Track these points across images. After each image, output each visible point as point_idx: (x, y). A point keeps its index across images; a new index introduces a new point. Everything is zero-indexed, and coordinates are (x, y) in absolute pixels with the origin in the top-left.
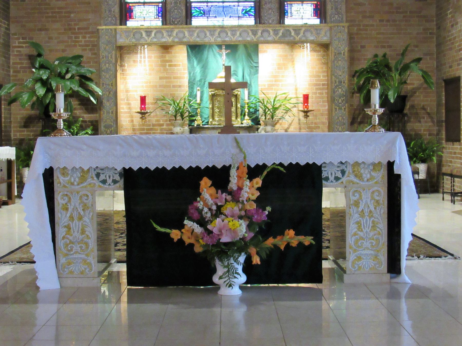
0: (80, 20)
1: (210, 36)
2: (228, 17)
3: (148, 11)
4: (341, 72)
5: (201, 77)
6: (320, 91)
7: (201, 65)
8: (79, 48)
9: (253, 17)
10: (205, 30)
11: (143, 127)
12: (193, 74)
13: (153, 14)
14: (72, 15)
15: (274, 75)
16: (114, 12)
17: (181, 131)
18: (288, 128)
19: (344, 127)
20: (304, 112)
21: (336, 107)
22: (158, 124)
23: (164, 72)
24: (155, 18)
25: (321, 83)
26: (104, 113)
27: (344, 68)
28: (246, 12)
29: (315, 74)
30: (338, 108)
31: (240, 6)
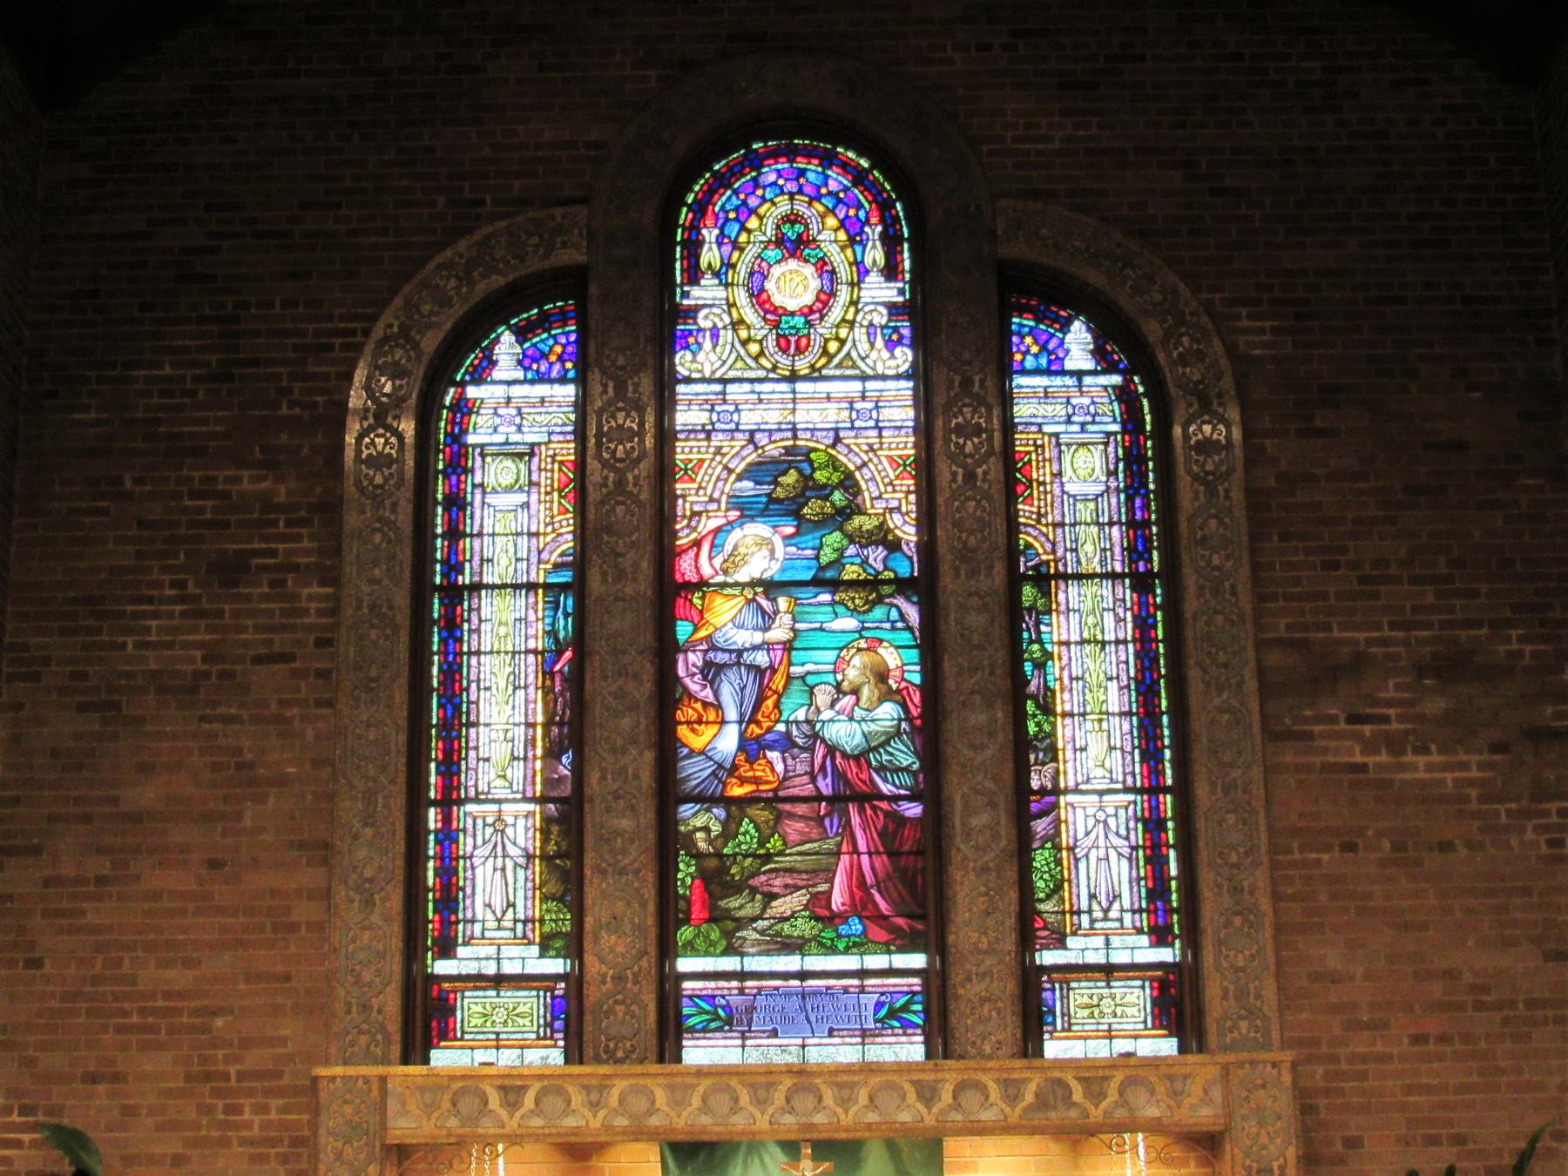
0: (246, 1044)
1: (751, 1108)
3: (511, 1007)
8: (240, 1149)
9: (919, 1031)
10: (734, 1082)
13: (532, 1021)
14: (219, 1022)
16: (379, 1011)
24: (538, 1038)
28: (892, 1014)
31: (867, 989)
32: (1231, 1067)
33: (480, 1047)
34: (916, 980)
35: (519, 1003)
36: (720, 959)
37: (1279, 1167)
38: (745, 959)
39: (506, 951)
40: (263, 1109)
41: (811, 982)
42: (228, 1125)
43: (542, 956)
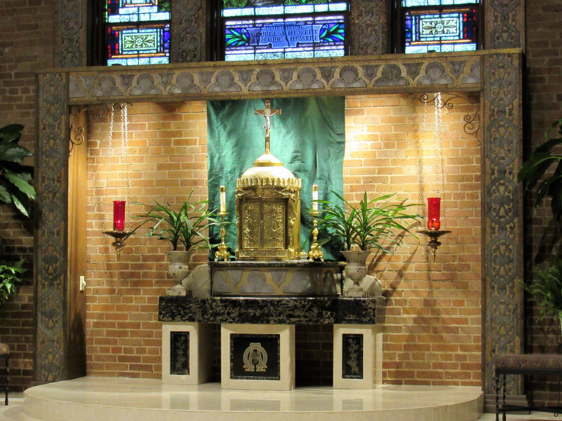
0: (19, 60)
1: (240, 83)
2: (294, 45)
3: (144, 38)
4: (504, 149)
5: (233, 163)
6: (470, 192)
7: (232, 141)
8: (17, 110)
9: (342, 43)
10: (231, 70)
11: (125, 262)
12: (219, 158)
13: (154, 44)
14: (7, 50)
15: (377, 158)
16: (77, 42)
17: (181, 270)
18: (405, 268)
19: (510, 266)
20: (431, 234)
21: (493, 225)
22: (153, 256)
23: (166, 156)
24: (157, 52)
25: (474, 174)
26: (43, 234)
27: (512, 142)
28: (329, 35)
29: (460, 156)
30: (497, 226)
31: (316, 22)
32: (486, 56)
33: (130, 58)
34: (341, 17)
35: (148, 35)
36: (244, 10)
37: (509, 110)
38: (256, 9)
39: (142, 10)
40: (26, 91)
41: (289, 20)
42: (11, 99)
43: (159, 11)
